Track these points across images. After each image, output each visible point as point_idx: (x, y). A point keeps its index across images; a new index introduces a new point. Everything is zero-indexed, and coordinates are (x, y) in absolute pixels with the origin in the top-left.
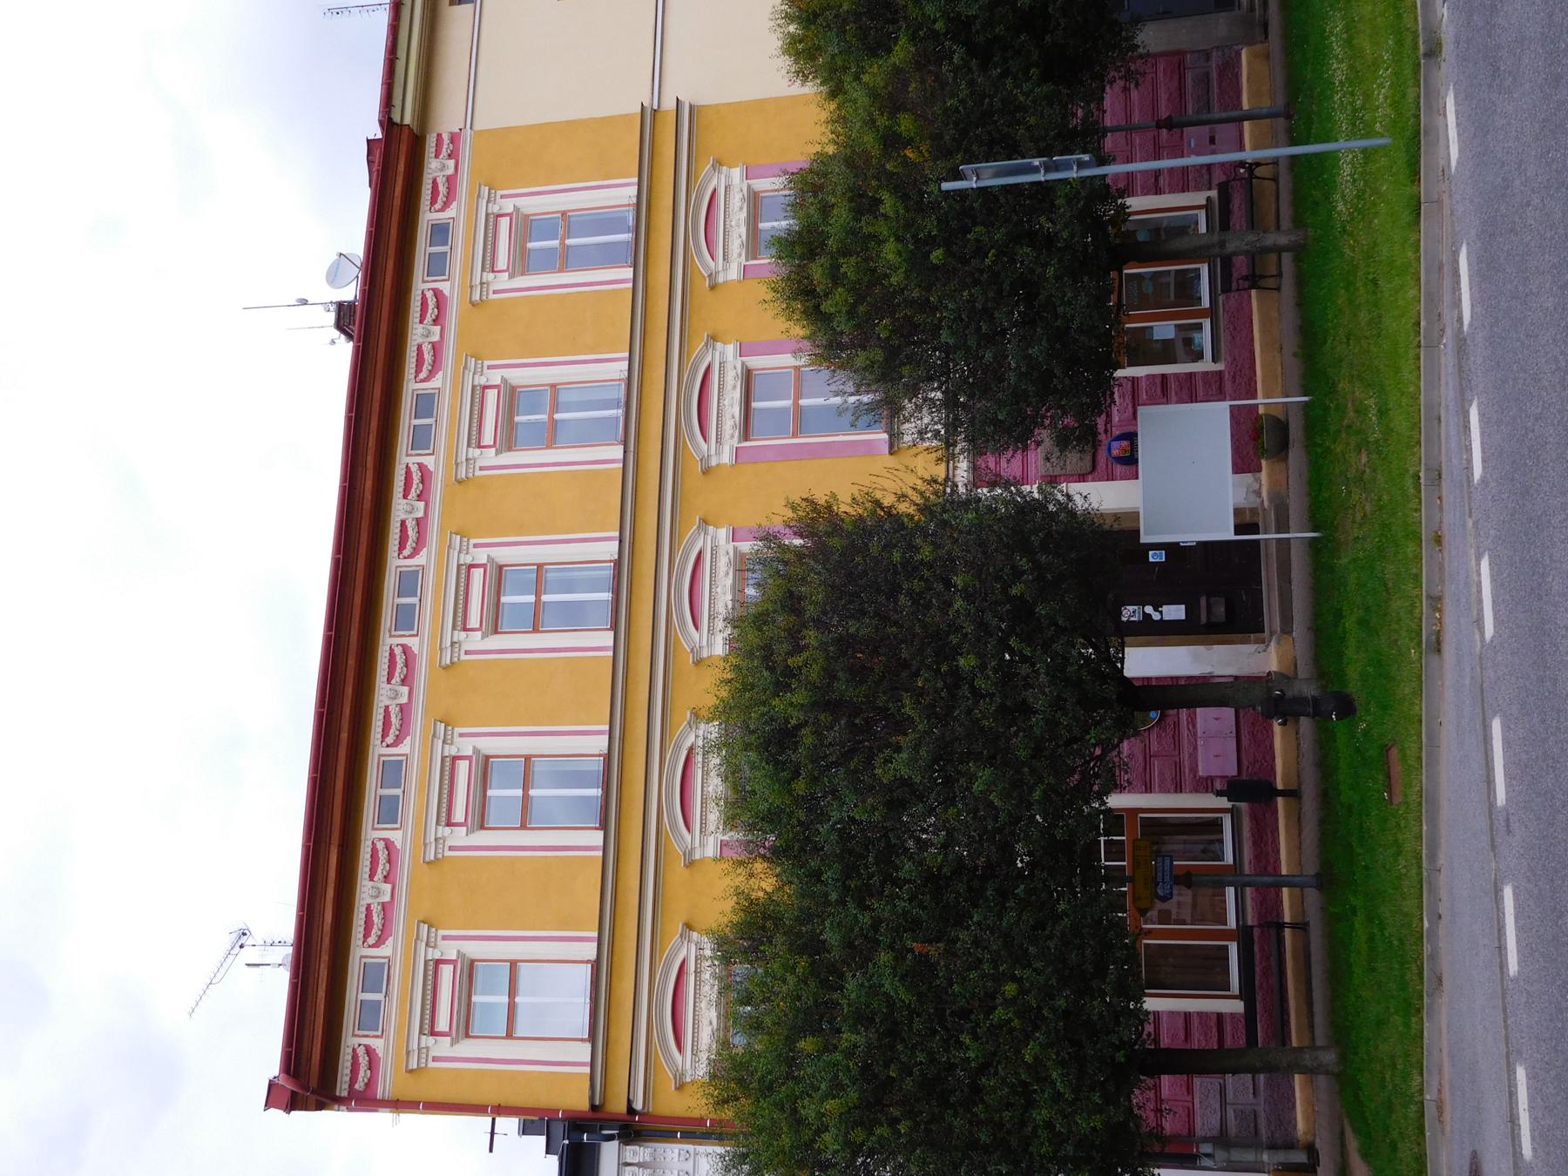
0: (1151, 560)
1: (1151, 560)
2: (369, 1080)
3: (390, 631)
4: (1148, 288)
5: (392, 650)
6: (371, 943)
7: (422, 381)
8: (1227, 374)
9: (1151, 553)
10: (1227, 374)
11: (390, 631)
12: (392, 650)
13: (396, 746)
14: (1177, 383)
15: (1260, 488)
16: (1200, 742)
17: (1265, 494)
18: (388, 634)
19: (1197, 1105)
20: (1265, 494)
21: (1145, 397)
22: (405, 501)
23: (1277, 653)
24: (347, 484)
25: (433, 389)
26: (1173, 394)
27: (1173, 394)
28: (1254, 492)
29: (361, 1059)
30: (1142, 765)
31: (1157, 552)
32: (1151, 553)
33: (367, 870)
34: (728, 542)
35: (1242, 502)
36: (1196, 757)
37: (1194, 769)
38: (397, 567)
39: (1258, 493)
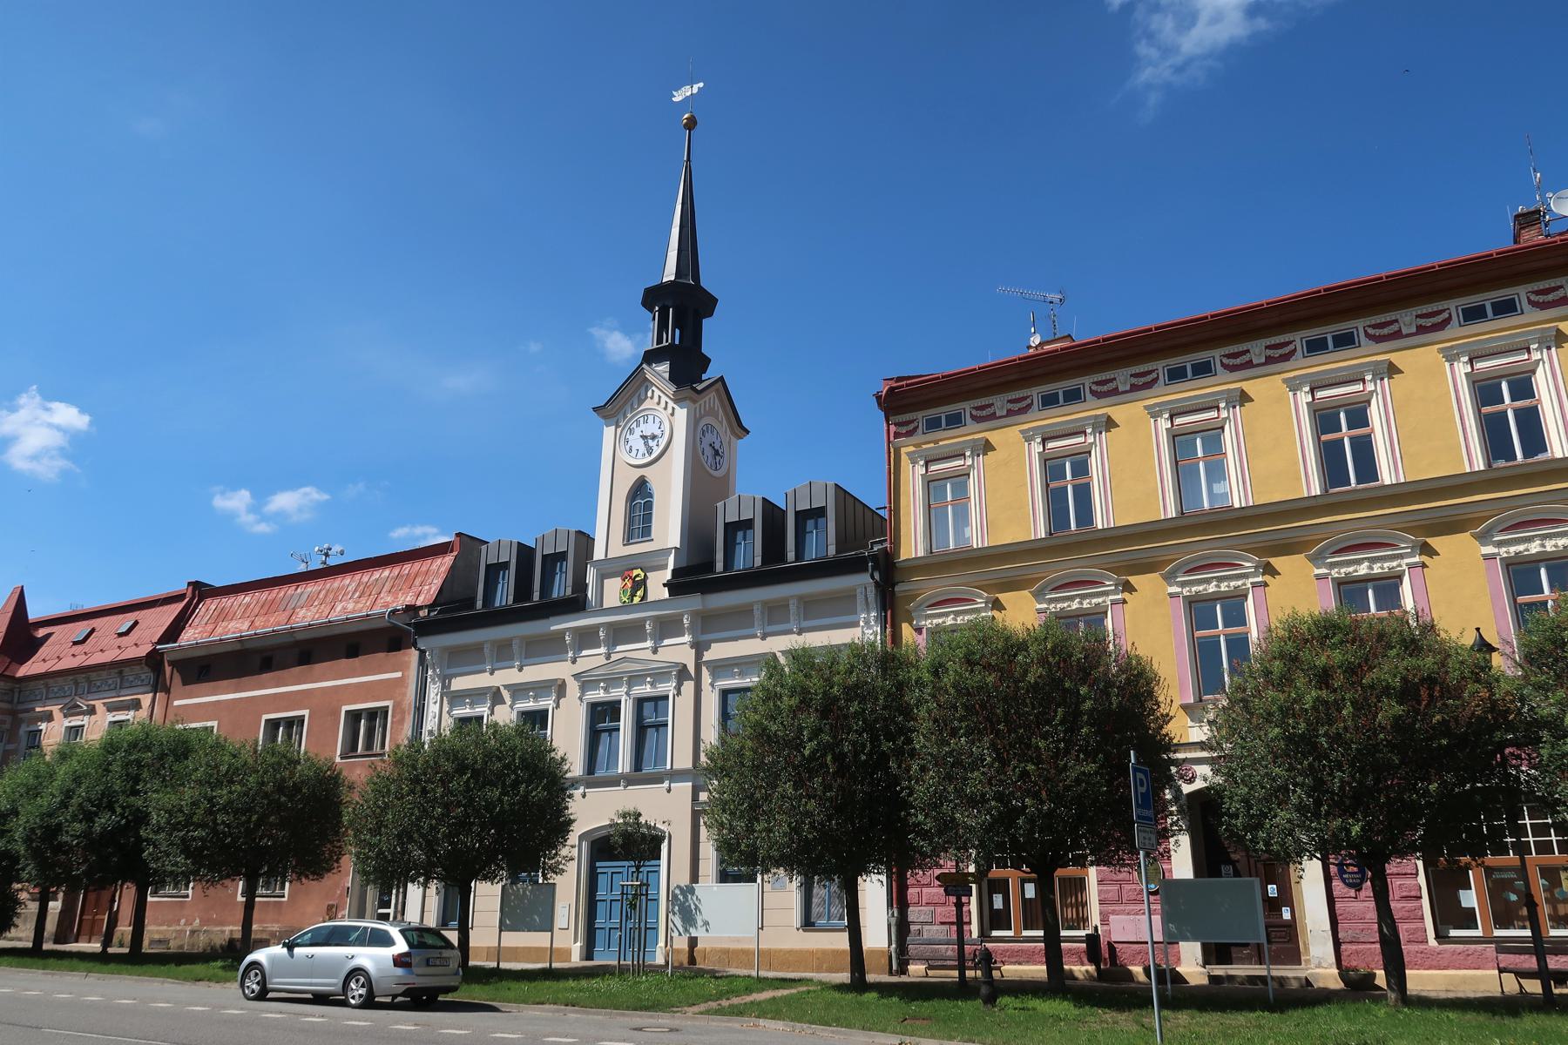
0: (1269, 886)
1: (1269, 886)
2: (1273, 357)
3: (1167, 366)
4: (386, 899)
5: (1291, 342)
6: (1224, 361)
7: (1365, 331)
8: (1425, 947)
9: (1275, 886)
10: (1425, 947)
11: (1167, 366)
12: (1291, 342)
13: (1091, 393)
14: (1413, 908)
15: (1323, 967)
16: (1132, 917)
17: (1318, 970)
18: (1165, 365)
19: (920, 908)
20: (1318, 970)
21: (1398, 883)
22: (1264, 348)
23: (1194, 972)
24: (1495, 256)
25: (1359, 341)
26: (1402, 905)
27: (1402, 905)
28: (1320, 963)
29: (1148, 377)
30: (1114, 879)
31: (1276, 891)
32: (1275, 886)
33: (1424, 311)
34: (1251, 583)
35: (52, 942)
36: (1122, 914)
37: (1114, 913)
38: (1518, 294)
39: (1319, 966)
